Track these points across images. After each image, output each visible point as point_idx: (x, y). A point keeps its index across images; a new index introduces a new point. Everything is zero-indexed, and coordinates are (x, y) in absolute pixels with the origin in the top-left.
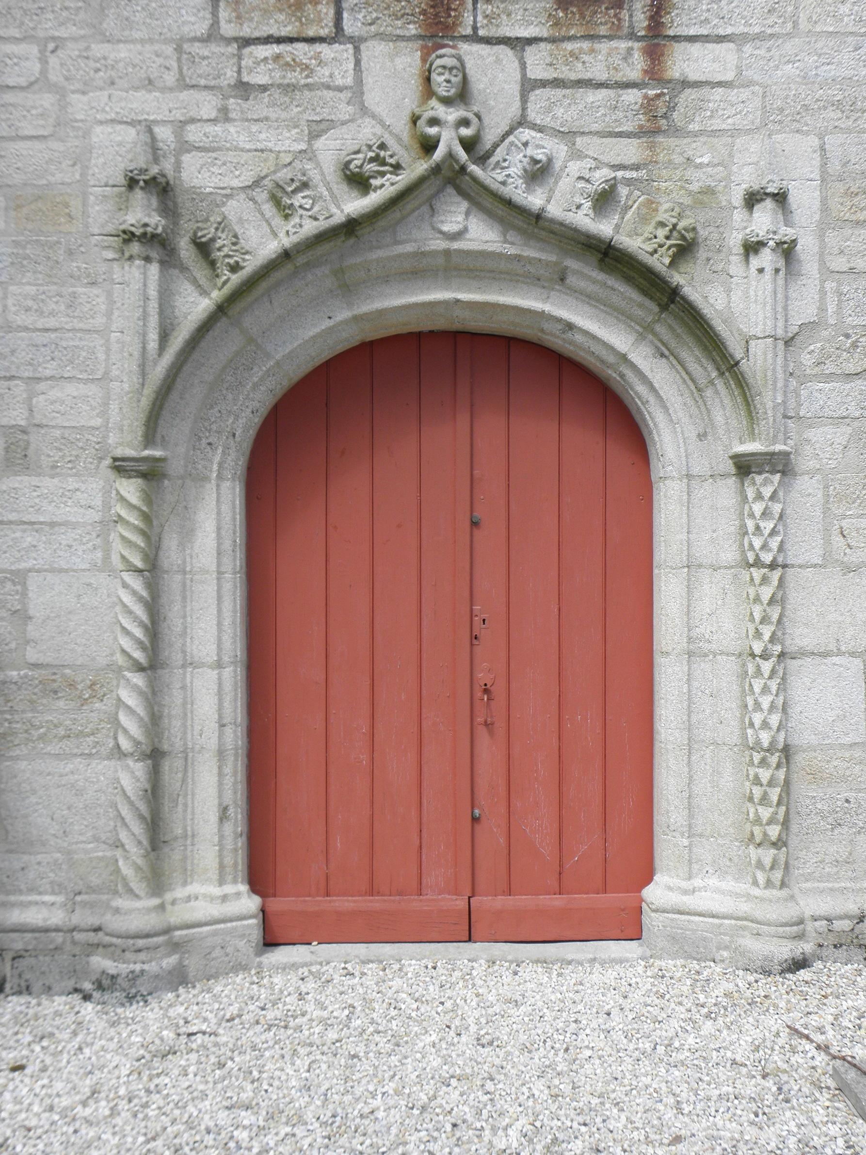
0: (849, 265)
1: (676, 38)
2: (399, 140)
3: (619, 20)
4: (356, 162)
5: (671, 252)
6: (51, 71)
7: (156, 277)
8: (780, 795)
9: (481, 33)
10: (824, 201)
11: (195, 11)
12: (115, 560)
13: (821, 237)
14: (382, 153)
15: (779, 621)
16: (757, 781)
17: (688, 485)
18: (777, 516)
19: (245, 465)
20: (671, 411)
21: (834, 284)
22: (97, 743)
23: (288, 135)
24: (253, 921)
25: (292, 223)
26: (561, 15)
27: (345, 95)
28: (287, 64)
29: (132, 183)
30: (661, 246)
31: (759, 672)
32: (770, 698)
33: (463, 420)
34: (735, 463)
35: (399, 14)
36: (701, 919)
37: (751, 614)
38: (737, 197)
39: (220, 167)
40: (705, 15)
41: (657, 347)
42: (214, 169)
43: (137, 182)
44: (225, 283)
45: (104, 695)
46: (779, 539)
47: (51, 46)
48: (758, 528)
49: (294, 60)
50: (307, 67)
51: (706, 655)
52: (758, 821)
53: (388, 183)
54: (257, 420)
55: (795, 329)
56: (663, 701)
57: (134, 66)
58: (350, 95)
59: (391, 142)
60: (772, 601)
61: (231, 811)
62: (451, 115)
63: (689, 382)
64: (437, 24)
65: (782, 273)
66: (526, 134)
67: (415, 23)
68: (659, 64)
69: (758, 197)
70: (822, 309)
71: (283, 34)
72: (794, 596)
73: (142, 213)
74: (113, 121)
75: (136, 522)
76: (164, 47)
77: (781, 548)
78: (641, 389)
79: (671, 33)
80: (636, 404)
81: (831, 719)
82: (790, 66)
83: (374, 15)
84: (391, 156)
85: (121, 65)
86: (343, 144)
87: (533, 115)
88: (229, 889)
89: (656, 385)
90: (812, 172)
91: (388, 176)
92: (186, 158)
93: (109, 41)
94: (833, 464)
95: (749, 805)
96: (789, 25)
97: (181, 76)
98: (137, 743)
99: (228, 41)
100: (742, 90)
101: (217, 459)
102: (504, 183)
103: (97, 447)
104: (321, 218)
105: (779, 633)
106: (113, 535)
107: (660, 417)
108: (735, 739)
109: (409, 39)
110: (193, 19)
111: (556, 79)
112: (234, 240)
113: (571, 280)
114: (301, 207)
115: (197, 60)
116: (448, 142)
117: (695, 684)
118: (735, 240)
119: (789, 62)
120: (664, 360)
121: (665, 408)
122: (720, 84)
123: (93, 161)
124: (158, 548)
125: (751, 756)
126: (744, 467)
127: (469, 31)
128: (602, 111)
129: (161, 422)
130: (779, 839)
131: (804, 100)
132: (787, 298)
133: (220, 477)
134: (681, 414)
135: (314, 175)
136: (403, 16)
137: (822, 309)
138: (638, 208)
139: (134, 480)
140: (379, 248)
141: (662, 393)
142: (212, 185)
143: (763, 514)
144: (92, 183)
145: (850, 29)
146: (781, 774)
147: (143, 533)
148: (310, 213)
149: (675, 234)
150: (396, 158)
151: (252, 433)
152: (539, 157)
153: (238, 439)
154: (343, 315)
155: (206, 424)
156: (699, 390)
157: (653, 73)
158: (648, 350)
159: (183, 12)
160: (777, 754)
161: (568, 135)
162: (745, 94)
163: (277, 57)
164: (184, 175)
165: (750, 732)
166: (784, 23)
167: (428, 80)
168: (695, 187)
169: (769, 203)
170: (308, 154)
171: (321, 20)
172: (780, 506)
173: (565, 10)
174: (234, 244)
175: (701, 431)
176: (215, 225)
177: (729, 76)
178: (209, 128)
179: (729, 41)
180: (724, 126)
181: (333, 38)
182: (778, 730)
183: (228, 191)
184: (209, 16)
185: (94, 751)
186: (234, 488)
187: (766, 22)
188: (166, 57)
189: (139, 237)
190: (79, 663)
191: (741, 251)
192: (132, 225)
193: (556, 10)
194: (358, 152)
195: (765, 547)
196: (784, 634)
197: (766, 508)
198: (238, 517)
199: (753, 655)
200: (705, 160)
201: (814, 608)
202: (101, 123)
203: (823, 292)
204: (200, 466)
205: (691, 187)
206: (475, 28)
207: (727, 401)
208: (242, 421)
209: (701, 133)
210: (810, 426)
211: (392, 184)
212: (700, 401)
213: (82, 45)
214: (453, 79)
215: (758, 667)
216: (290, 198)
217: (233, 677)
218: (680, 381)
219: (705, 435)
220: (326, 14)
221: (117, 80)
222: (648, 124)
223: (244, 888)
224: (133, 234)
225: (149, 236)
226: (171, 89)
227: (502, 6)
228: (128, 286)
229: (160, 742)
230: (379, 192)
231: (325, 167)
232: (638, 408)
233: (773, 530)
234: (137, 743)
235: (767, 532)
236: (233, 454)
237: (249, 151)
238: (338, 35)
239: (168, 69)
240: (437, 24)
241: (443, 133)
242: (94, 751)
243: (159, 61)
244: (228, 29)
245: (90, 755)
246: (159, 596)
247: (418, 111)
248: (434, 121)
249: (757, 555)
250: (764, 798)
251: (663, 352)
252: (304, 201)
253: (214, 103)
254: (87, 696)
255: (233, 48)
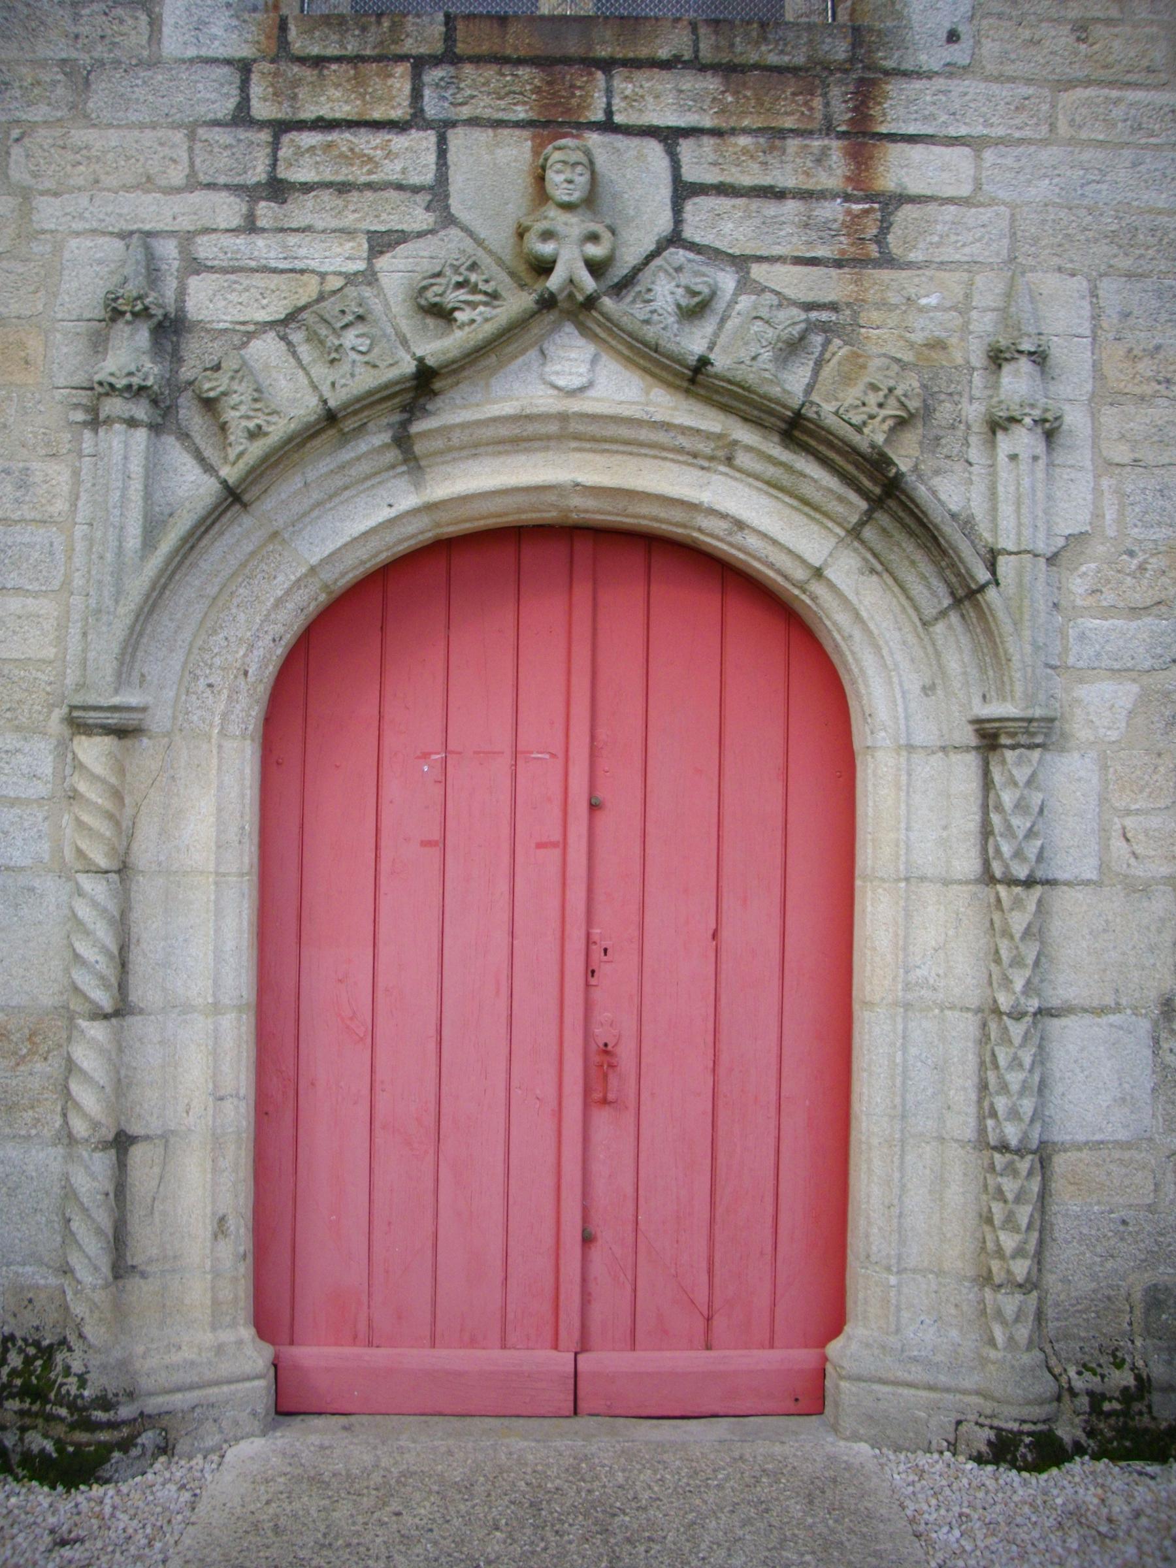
0: (1132, 456)
1: (893, 138)
2: (500, 262)
3: (811, 109)
4: (435, 288)
5: (886, 427)
6: (12, 165)
7: (143, 447)
8: (1032, 1216)
9: (618, 119)
10: (1096, 366)
11: (216, 85)
12: (69, 854)
13: (1094, 416)
14: (473, 277)
15: (1037, 963)
16: (1000, 1194)
17: (908, 760)
18: (1037, 809)
19: (262, 716)
20: (885, 652)
21: (1113, 482)
22: (38, 1120)
23: (339, 250)
24: (261, 1383)
25: (341, 372)
26: (730, 99)
27: (423, 198)
28: (342, 155)
29: (116, 314)
30: (872, 417)
31: (1006, 1038)
32: (1021, 1076)
33: (582, 592)
34: (977, 731)
35: (503, 92)
36: (913, 1391)
37: (997, 952)
38: (978, 358)
39: (240, 293)
40: (932, 108)
41: (865, 559)
42: (233, 297)
43: (123, 313)
44: (240, 455)
45: (48, 1052)
46: (1039, 843)
47: (16, 133)
48: (1009, 827)
49: (352, 150)
50: (370, 159)
51: (930, 1009)
52: (999, 1253)
53: (479, 319)
54: (280, 651)
55: (1061, 542)
56: (865, 1074)
57: (128, 158)
58: (429, 198)
59: (486, 261)
60: (1027, 933)
61: (231, 1223)
62: (573, 225)
63: (911, 611)
64: (555, 105)
65: (1042, 463)
66: (679, 255)
67: (524, 103)
68: (867, 170)
69: (1007, 355)
70: (1097, 515)
71: (338, 115)
72: (1057, 927)
73: (129, 354)
74: (94, 231)
75: (100, 801)
76: (170, 133)
77: (1040, 857)
78: (842, 618)
79: (883, 129)
80: (834, 640)
81: (1105, 1105)
82: (1047, 181)
83: (469, 92)
84: (487, 281)
85: (110, 156)
86: (417, 264)
87: (689, 233)
88: (227, 1336)
89: (864, 614)
90: (1080, 325)
91: (481, 308)
92: (193, 282)
93: (94, 125)
94: (1113, 735)
95: (987, 1228)
96: (1044, 129)
97: (193, 172)
98: (95, 1125)
99: (262, 124)
100: (981, 210)
101: (221, 707)
102: (647, 322)
103: (48, 689)
104: (382, 365)
105: (1036, 980)
106: (66, 817)
107: (868, 660)
108: (969, 1133)
109: (518, 124)
110: (213, 96)
111: (722, 184)
112: (256, 395)
113: (742, 459)
114: (353, 349)
115: (216, 150)
116: (570, 267)
117: (913, 1051)
118: (974, 412)
119: (1045, 176)
120: (875, 578)
121: (877, 649)
122: (950, 201)
123: (64, 286)
124: (131, 836)
125: (992, 1158)
126: (990, 739)
127: (600, 116)
128: (789, 229)
129: (140, 654)
130: (1027, 1280)
131: (1067, 228)
132: (1049, 498)
133: (223, 733)
134: (899, 657)
135: (376, 305)
136: (507, 94)
137: (1097, 515)
138: (839, 363)
139: (98, 739)
140: (464, 407)
141: (872, 626)
142: (228, 318)
143: (1017, 806)
144: (59, 316)
145: (1125, 138)
146: (1035, 1186)
147: (111, 817)
148: (366, 358)
149: (892, 401)
150: (492, 283)
151: (271, 670)
152: (698, 288)
153: (251, 678)
154: (408, 500)
155: (207, 657)
156: (925, 624)
157: (858, 182)
158: (852, 562)
159: (200, 86)
160: (1030, 1157)
161: (741, 262)
162: (986, 214)
163: (329, 146)
164: (190, 305)
165: (990, 1123)
166: (1037, 125)
167: (541, 179)
168: (918, 337)
169: (1024, 364)
170: (370, 277)
171: (393, 98)
172: (1040, 796)
173: (736, 93)
174: (255, 400)
175: (928, 682)
176: (230, 374)
177: (965, 190)
178: (228, 241)
179: (963, 144)
180: (957, 257)
181: (407, 122)
182: (1032, 1121)
183: (251, 328)
184: (236, 92)
185: (33, 1132)
186: (243, 751)
187: (1012, 122)
188: (173, 146)
189: (121, 391)
190: (14, 1003)
191: (985, 429)
192: (112, 374)
193: (723, 92)
194: (439, 275)
195: (1018, 854)
196: (1042, 981)
197: (1022, 798)
198: (248, 792)
199: (996, 1011)
200: (933, 300)
201: (1084, 944)
202: (78, 234)
203: (1097, 491)
204: (195, 718)
205: (912, 337)
206: (609, 112)
207: (964, 640)
208: (258, 653)
209: (927, 264)
210: (1081, 681)
211: (487, 320)
212: (926, 639)
213: (59, 132)
214: (578, 179)
215: (1006, 1029)
216: (339, 336)
217: (235, 1033)
218: (897, 610)
219: (933, 687)
220: (400, 90)
221: (103, 177)
222: (852, 249)
223: (247, 1333)
224: (111, 385)
225: (135, 387)
226: (178, 190)
227: (647, 85)
228: (102, 459)
229: (128, 1121)
230: (467, 329)
231: (389, 294)
232: (837, 646)
233: (1030, 830)
234: (95, 1125)
235: (1021, 834)
236: (243, 700)
237: (283, 271)
238: (415, 120)
239: (174, 161)
240: (555, 105)
241: (562, 252)
242: (33, 1132)
243: (166, 151)
244: (261, 109)
245: (28, 1137)
246: (130, 909)
247: (527, 222)
248: (547, 235)
249: (1007, 866)
250: (1010, 1218)
251: (879, 566)
252: (360, 340)
253: (237, 208)
254: (25, 1051)
255: (265, 136)
